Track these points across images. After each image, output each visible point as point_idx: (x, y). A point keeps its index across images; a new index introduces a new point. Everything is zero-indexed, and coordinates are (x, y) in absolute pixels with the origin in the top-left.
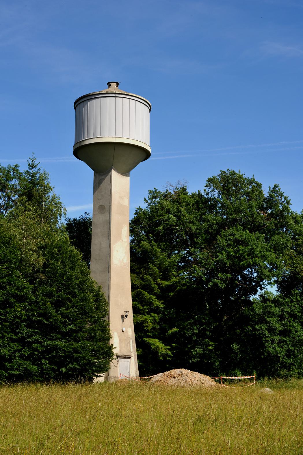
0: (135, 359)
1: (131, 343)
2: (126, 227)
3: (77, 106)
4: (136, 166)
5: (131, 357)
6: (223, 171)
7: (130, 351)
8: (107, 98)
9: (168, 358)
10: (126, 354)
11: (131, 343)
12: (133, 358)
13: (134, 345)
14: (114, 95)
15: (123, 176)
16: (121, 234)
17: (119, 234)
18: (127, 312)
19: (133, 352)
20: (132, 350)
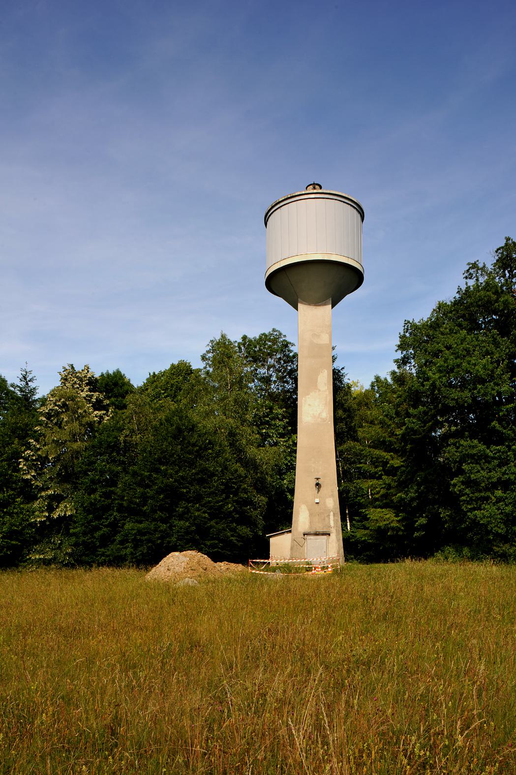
0: (337, 535)
1: (332, 517)
2: (326, 371)
3: (267, 220)
4: (359, 287)
5: (329, 534)
6: (97, 372)
7: (330, 527)
8: (287, 205)
9: (400, 533)
10: (325, 530)
11: (332, 517)
12: (333, 536)
13: (336, 518)
14: (278, 206)
15: (318, 307)
16: (317, 382)
17: (313, 384)
18: (318, 479)
19: (334, 527)
20: (332, 523)
